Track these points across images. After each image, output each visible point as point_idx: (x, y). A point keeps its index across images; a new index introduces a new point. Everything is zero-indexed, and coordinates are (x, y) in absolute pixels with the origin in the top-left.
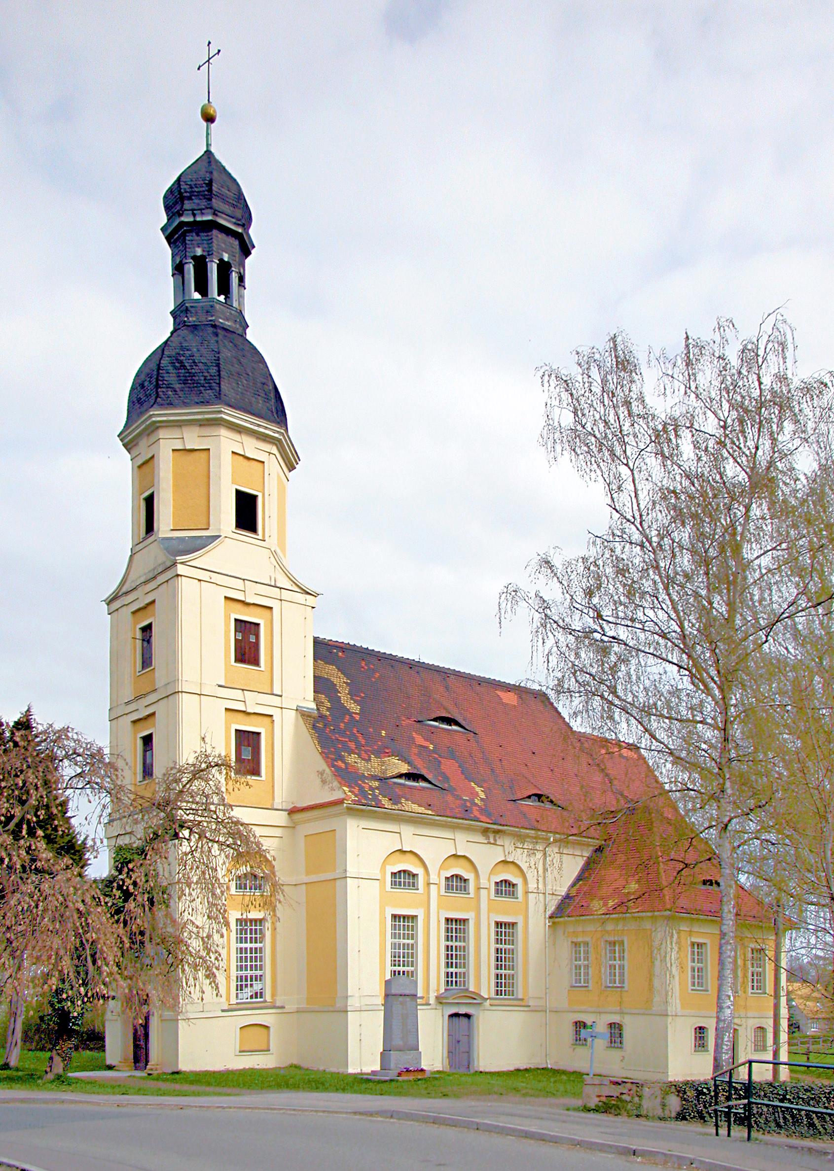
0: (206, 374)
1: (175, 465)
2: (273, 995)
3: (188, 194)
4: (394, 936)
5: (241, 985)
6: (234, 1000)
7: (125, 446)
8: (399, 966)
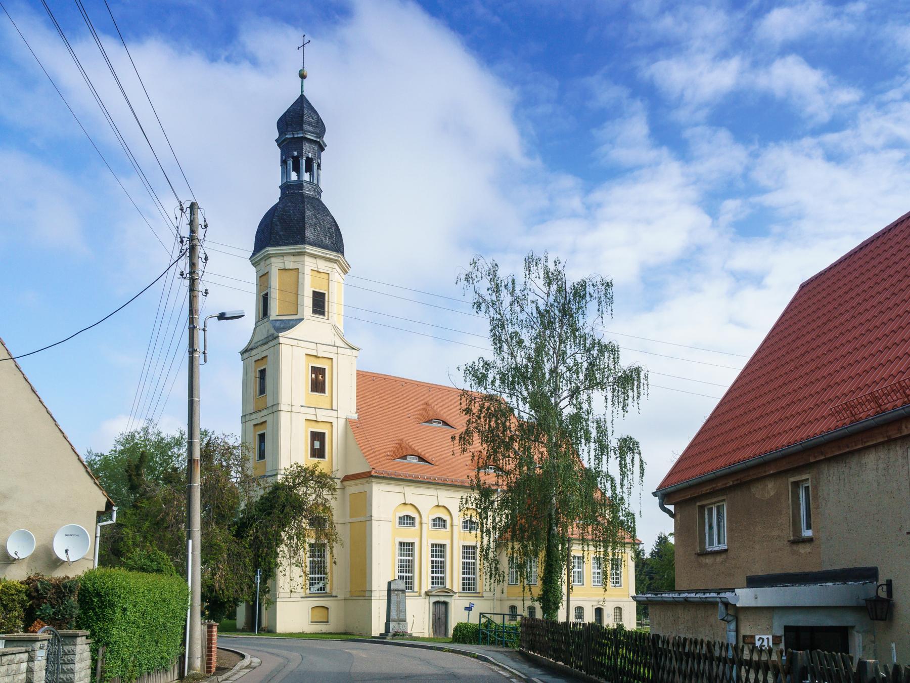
0: (297, 226)
1: (280, 278)
2: (331, 589)
4: (401, 555)
7: (253, 264)
8: (403, 572)
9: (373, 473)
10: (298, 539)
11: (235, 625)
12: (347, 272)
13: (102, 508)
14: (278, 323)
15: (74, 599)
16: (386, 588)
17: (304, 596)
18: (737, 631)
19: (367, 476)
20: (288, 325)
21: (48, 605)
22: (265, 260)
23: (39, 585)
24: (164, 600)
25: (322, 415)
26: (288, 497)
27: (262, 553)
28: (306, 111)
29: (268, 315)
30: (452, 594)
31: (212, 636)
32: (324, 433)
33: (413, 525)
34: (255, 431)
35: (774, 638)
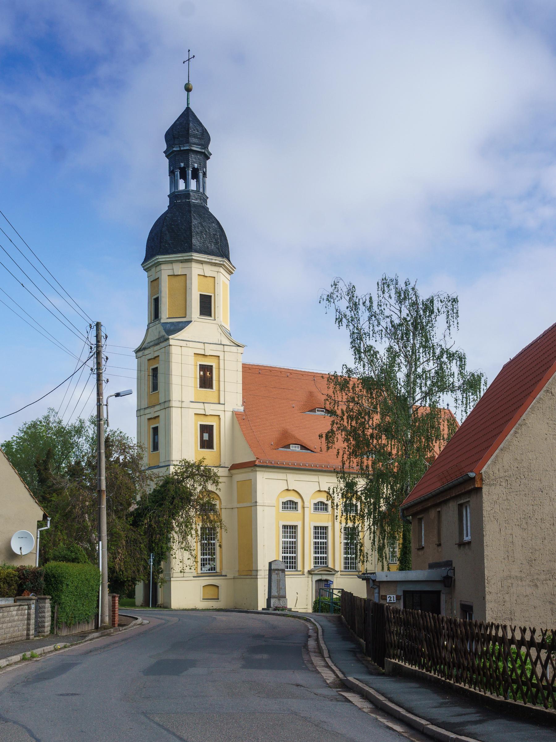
0: (185, 235)
2: (221, 569)
3: (177, 136)
4: (285, 537)
5: (204, 563)
6: (199, 571)
7: (145, 270)
8: (287, 553)
9: (257, 463)
10: (186, 526)
11: (134, 603)
12: (232, 273)
13: (41, 519)
14: (169, 325)
15: (42, 579)
16: (267, 568)
18: (379, 593)
19: (251, 466)
20: (177, 327)
21: (30, 582)
22: (156, 267)
23: (24, 571)
24: (87, 580)
25: (210, 409)
26: (177, 490)
27: (155, 540)
28: (191, 125)
29: (159, 318)
30: (333, 573)
31: (115, 603)
32: (212, 426)
33: (295, 509)
34: (149, 426)
35: (397, 596)
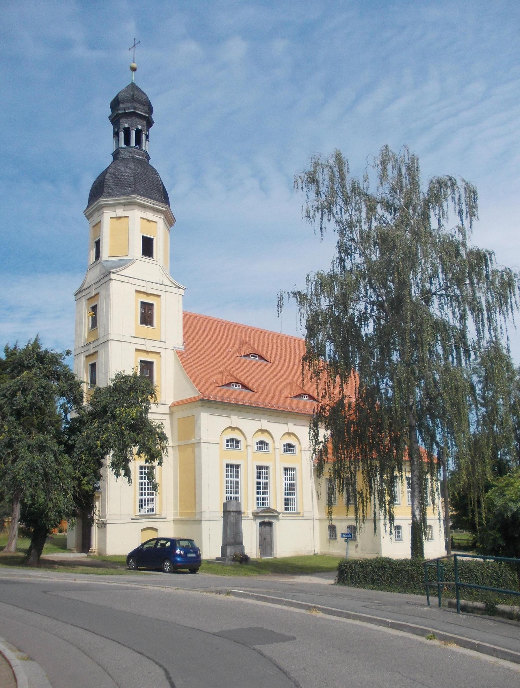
8: (231, 493)
17: (134, 517)
30: (276, 514)
